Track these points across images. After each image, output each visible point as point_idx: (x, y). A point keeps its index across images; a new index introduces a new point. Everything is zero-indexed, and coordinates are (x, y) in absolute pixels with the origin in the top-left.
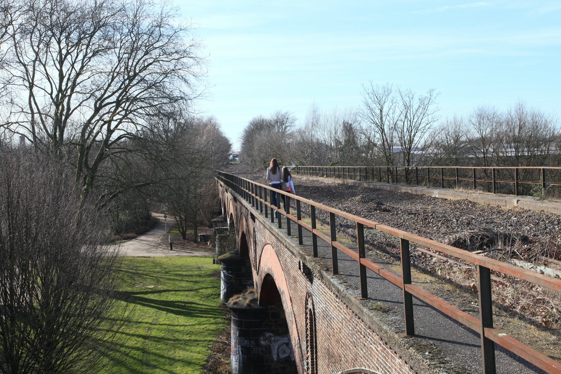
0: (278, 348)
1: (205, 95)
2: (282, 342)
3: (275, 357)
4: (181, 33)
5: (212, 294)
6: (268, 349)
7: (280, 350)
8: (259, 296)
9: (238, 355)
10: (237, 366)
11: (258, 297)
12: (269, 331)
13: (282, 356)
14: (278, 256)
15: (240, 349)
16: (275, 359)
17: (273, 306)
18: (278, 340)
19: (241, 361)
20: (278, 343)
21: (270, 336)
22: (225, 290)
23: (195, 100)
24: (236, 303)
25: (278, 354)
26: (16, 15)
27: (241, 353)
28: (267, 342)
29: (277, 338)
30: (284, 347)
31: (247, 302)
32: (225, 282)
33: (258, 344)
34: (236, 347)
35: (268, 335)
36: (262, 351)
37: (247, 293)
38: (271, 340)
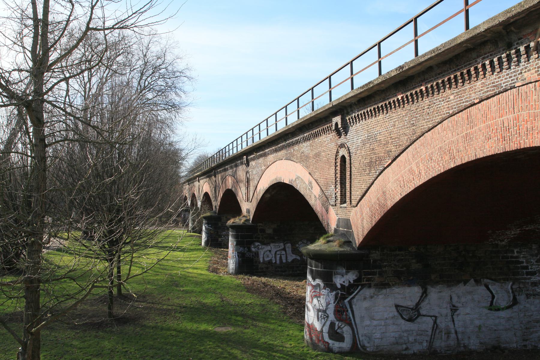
0: (264, 254)
1: (193, 104)
2: (266, 249)
3: (261, 260)
4: (178, 61)
5: (194, 244)
6: (257, 254)
7: (265, 255)
8: (251, 217)
9: (235, 259)
10: (234, 267)
11: (250, 218)
12: (258, 241)
13: (267, 259)
14: (289, 160)
15: (237, 254)
16: (262, 261)
17: (261, 224)
18: (264, 248)
19: (237, 263)
20: (264, 250)
21: (258, 245)
22: (206, 239)
23: (186, 109)
24: (233, 223)
25: (263, 258)
26: (19, 156)
27: (237, 257)
28: (256, 249)
29: (263, 246)
30: (268, 252)
31: (242, 221)
32: (206, 233)
33: (250, 250)
34: (233, 253)
35: (257, 244)
36: (253, 256)
37: (241, 217)
38: (259, 248)
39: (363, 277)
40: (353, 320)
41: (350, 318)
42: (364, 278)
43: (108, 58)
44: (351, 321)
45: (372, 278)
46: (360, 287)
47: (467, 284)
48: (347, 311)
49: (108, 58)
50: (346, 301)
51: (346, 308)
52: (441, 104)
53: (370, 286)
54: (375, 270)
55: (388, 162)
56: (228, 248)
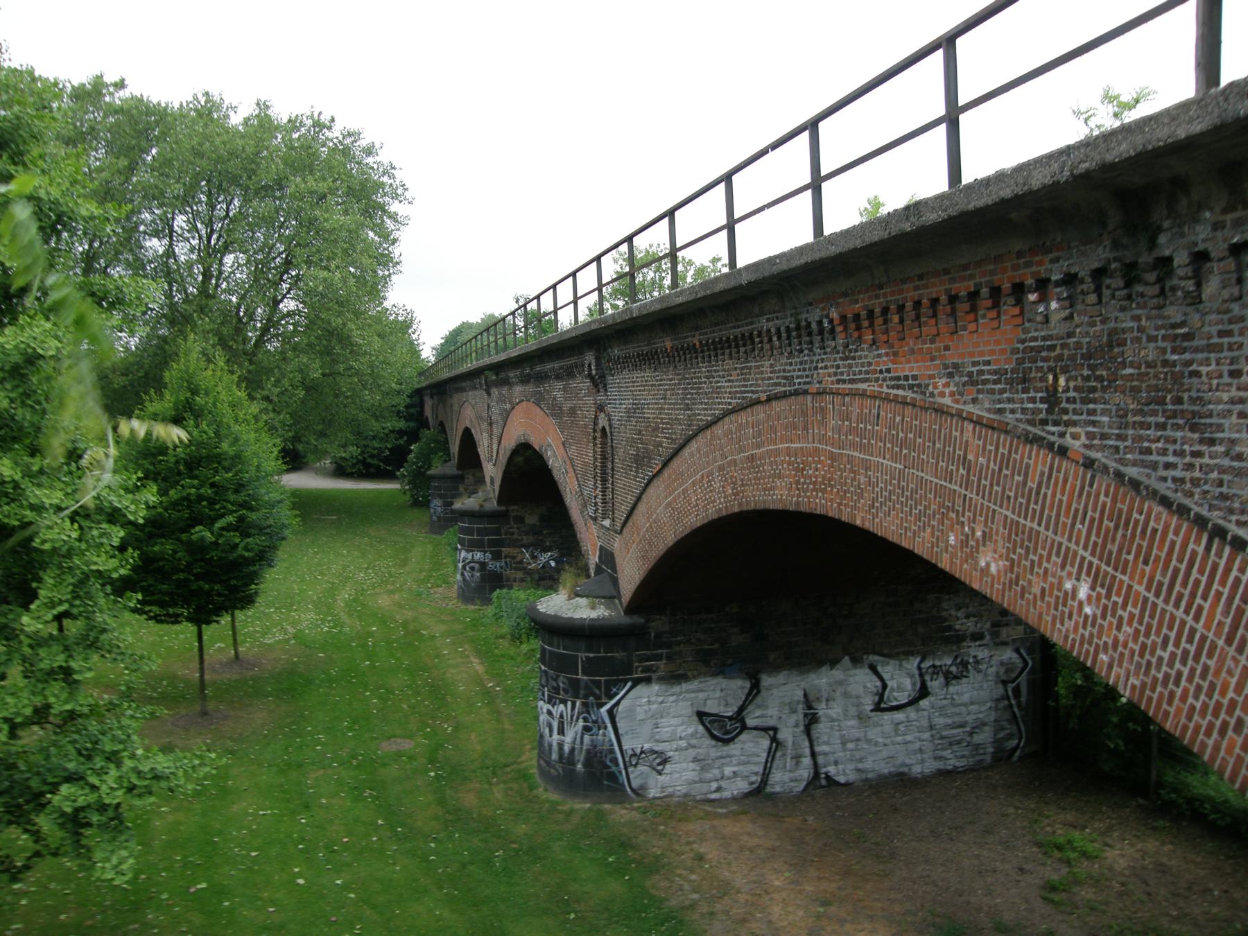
36: (501, 567)
39: (636, 664)
41: (610, 740)
44: (612, 745)
46: (629, 684)
48: (606, 728)
50: (604, 710)
51: (604, 722)
53: (648, 681)
54: (660, 651)
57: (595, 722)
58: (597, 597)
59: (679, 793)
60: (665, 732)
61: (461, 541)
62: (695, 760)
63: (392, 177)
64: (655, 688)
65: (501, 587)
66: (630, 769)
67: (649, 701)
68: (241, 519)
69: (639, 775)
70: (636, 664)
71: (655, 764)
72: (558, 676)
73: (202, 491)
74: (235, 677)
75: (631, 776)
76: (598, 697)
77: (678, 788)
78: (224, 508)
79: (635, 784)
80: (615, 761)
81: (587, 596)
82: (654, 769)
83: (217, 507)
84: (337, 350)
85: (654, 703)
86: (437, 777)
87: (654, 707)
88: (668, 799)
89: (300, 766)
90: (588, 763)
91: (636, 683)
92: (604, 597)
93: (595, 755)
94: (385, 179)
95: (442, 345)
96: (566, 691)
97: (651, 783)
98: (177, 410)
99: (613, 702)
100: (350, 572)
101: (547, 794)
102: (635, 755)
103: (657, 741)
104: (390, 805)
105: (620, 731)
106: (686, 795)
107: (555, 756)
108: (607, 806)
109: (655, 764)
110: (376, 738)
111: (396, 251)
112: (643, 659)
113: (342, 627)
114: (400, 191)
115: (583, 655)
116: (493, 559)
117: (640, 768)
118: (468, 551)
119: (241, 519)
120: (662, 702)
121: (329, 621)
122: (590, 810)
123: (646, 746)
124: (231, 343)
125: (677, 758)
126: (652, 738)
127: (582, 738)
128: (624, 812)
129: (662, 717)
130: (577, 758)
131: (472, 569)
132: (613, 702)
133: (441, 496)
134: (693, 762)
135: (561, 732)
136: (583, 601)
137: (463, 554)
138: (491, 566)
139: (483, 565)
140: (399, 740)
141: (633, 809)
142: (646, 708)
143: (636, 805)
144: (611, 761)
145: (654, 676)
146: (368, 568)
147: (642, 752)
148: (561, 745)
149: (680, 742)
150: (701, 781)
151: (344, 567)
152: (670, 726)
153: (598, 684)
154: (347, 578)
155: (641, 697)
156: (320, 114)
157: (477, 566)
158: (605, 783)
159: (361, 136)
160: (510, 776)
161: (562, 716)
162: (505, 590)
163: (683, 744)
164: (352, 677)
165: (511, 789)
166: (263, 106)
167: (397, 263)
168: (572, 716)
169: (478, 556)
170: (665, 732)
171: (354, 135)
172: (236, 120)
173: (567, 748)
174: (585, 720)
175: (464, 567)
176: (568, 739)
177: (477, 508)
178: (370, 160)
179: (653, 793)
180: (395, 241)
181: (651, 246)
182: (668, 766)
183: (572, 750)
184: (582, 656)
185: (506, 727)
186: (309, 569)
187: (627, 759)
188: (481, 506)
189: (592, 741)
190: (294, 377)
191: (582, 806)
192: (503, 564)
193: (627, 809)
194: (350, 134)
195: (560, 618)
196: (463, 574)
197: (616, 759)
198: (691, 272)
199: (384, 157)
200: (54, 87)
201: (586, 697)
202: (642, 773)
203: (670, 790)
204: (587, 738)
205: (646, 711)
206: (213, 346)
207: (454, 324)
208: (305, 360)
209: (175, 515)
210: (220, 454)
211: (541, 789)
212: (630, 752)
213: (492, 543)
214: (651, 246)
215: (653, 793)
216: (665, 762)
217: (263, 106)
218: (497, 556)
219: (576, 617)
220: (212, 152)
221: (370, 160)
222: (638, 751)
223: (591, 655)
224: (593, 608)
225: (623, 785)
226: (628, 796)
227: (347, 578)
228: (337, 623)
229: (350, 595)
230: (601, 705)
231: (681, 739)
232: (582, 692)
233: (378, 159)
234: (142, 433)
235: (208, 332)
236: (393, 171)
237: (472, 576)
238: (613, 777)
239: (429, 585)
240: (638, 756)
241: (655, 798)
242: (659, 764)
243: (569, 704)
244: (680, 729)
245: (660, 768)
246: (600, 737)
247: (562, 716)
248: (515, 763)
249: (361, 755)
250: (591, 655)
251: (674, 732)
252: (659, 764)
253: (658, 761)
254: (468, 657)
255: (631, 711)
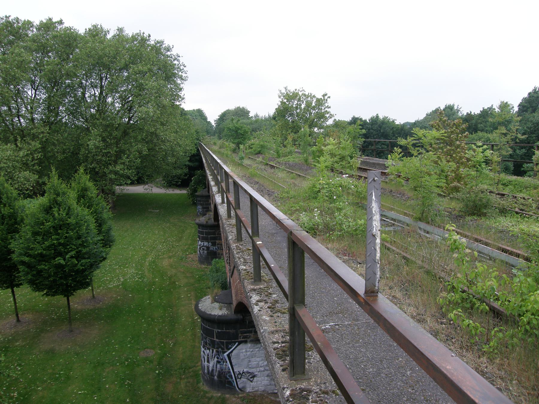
36: (216, 249)
39: (240, 335)
40: (231, 371)
41: (229, 367)
42: (240, 336)
43: (20, 54)
44: (230, 369)
45: (247, 335)
46: (237, 343)
47: (186, 160)
48: (226, 362)
49: (20, 54)
50: (226, 354)
51: (226, 360)
52: (239, 238)
53: (246, 342)
54: (251, 329)
55: (253, 202)
56: (221, 240)
57: (222, 359)
58: (223, 303)
59: (261, 390)
60: (254, 363)
61: (199, 237)
62: (268, 376)
63: (178, 61)
64: (249, 345)
65: (216, 258)
66: (238, 380)
67: (246, 351)
68: (79, 252)
69: (241, 382)
70: (240, 335)
71: (249, 378)
72: (206, 338)
73: (60, 241)
74: (92, 307)
75: (239, 383)
76: (223, 349)
77: (260, 388)
78: (71, 247)
79: (240, 386)
80: (231, 376)
81: (220, 303)
82: (249, 380)
83: (68, 247)
84: (155, 141)
85: (248, 352)
86: (158, 374)
87: (249, 353)
88: (256, 392)
89: (103, 364)
90: (219, 376)
91: (240, 343)
92: (226, 304)
93: (222, 373)
94: (176, 62)
95: (219, 119)
96: (210, 345)
97: (248, 386)
98: (50, 202)
99: (230, 351)
100: (156, 245)
101: (204, 387)
102: (240, 374)
103: (250, 368)
104: (135, 390)
105: (233, 364)
106: (263, 391)
107: (206, 371)
108: (227, 396)
109: (249, 378)
110: (139, 349)
111: (182, 94)
112: (242, 333)
113: (144, 278)
114: (182, 67)
115: (216, 330)
116: (212, 245)
117: (242, 379)
118: (202, 242)
119: (79, 252)
120: (252, 351)
121: (140, 274)
122: (220, 397)
123: (245, 370)
124: (108, 140)
125: (259, 375)
126: (248, 366)
127: (216, 366)
128: (234, 399)
129: (252, 358)
130: (215, 374)
131: (203, 249)
132: (230, 351)
133: (201, 205)
134: (267, 377)
135: (208, 362)
136: (217, 305)
137: (200, 242)
138: (212, 248)
139: (208, 248)
140: (148, 350)
141: (238, 398)
142: (245, 354)
143: (240, 395)
144: (229, 376)
145: (248, 340)
146: (164, 242)
147: (243, 373)
148: (208, 367)
149: (261, 368)
150: (270, 385)
151: (155, 241)
152: (256, 361)
153: (223, 343)
154: (154, 248)
155: (242, 349)
156: (144, 33)
157: (205, 248)
158: (227, 385)
159: (164, 43)
160: (191, 374)
161: (208, 355)
162: (217, 259)
163: (262, 369)
164: (140, 310)
165: (189, 382)
166: (120, 30)
167: (183, 99)
168: (212, 356)
169: (206, 244)
170: (254, 363)
171: (161, 42)
172: (109, 36)
173: (210, 369)
174: (218, 358)
175: (200, 248)
176: (211, 365)
177: (205, 223)
178: (169, 53)
179: (248, 390)
180: (181, 90)
181: (296, 90)
182: (255, 378)
183: (213, 370)
184: (216, 330)
185: (196, 344)
186: (139, 243)
187: (236, 376)
188: (207, 222)
189: (221, 367)
190: (136, 154)
191: (217, 394)
192: (217, 247)
193: (236, 397)
194: (158, 42)
195: (205, 313)
196: (200, 251)
197: (231, 376)
198: (315, 100)
199: (174, 52)
200: (28, 24)
201: (218, 348)
202: (244, 382)
203: (257, 389)
204: (218, 366)
205: (245, 355)
206: (99, 141)
207: (227, 109)
208: (140, 146)
209: (48, 253)
210: (68, 224)
211: (201, 384)
212: (238, 373)
213: (212, 239)
214: (296, 90)
215: (248, 390)
216: (254, 377)
217: (120, 30)
218: (214, 244)
219: (213, 314)
220: (96, 55)
221: (169, 53)
222: (241, 372)
223: (220, 331)
224: (221, 309)
225: (235, 387)
226: (237, 391)
227: (154, 248)
228: (143, 276)
229: (152, 258)
230: (224, 352)
231: (261, 367)
232: (216, 346)
233: (172, 53)
234: (64, 185)
235: (97, 136)
236: (179, 58)
237: (203, 252)
238: (230, 383)
239: (187, 253)
240: (241, 374)
241: (249, 392)
242: (251, 378)
243: (211, 350)
244: (261, 363)
245: (252, 379)
246: (224, 366)
247: (208, 355)
248: (195, 366)
249: (130, 359)
250: (220, 331)
251: (258, 364)
252: (251, 378)
253: (251, 376)
254: (191, 300)
255: (238, 355)
